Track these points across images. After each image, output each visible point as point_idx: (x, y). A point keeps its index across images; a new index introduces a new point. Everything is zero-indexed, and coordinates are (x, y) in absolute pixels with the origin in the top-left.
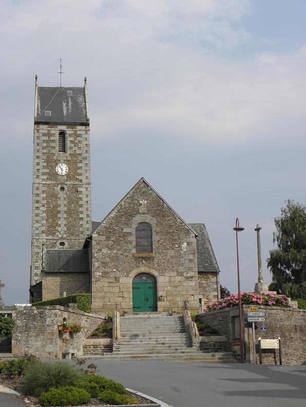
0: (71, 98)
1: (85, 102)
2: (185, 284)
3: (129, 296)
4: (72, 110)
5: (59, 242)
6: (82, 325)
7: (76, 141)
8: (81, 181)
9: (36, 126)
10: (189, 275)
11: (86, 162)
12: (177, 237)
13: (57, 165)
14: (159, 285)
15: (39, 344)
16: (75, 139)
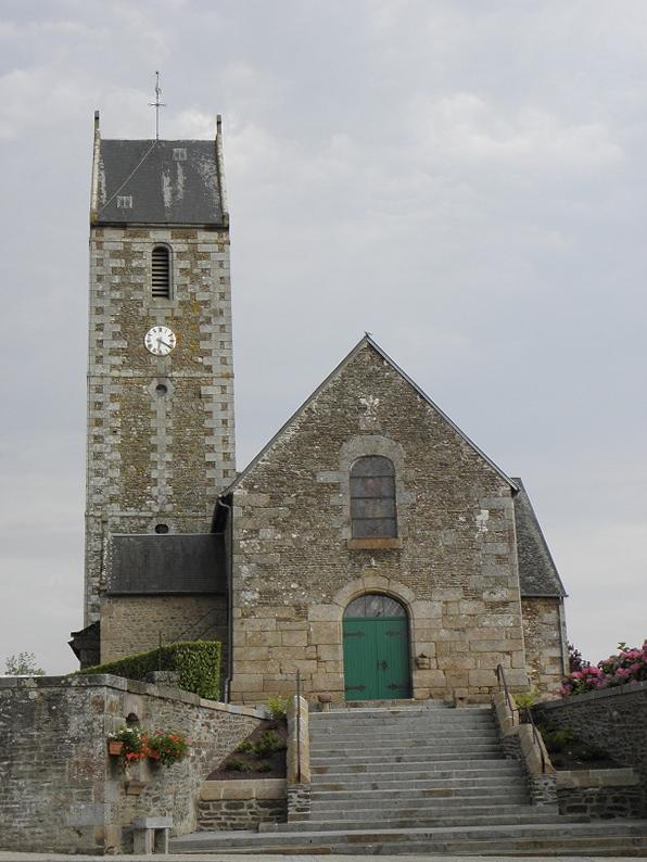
0: (184, 164)
1: (219, 175)
2: (487, 623)
3: (335, 656)
4: (185, 194)
5: (155, 522)
6: (193, 737)
7: (195, 271)
8: (209, 369)
9: (94, 231)
10: (497, 597)
11: (222, 321)
12: (460, 495)
13: (147, 329)
14: (415, 624)
15: (44, 800)
16: (194, 265)
